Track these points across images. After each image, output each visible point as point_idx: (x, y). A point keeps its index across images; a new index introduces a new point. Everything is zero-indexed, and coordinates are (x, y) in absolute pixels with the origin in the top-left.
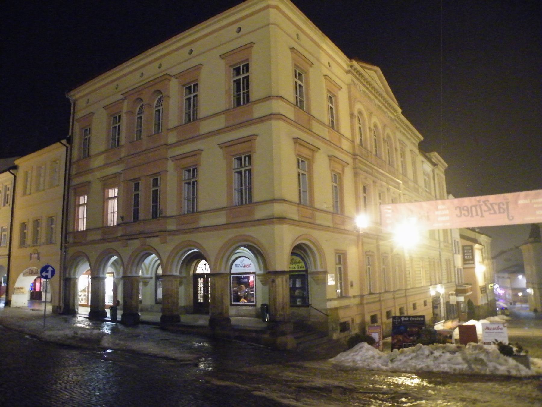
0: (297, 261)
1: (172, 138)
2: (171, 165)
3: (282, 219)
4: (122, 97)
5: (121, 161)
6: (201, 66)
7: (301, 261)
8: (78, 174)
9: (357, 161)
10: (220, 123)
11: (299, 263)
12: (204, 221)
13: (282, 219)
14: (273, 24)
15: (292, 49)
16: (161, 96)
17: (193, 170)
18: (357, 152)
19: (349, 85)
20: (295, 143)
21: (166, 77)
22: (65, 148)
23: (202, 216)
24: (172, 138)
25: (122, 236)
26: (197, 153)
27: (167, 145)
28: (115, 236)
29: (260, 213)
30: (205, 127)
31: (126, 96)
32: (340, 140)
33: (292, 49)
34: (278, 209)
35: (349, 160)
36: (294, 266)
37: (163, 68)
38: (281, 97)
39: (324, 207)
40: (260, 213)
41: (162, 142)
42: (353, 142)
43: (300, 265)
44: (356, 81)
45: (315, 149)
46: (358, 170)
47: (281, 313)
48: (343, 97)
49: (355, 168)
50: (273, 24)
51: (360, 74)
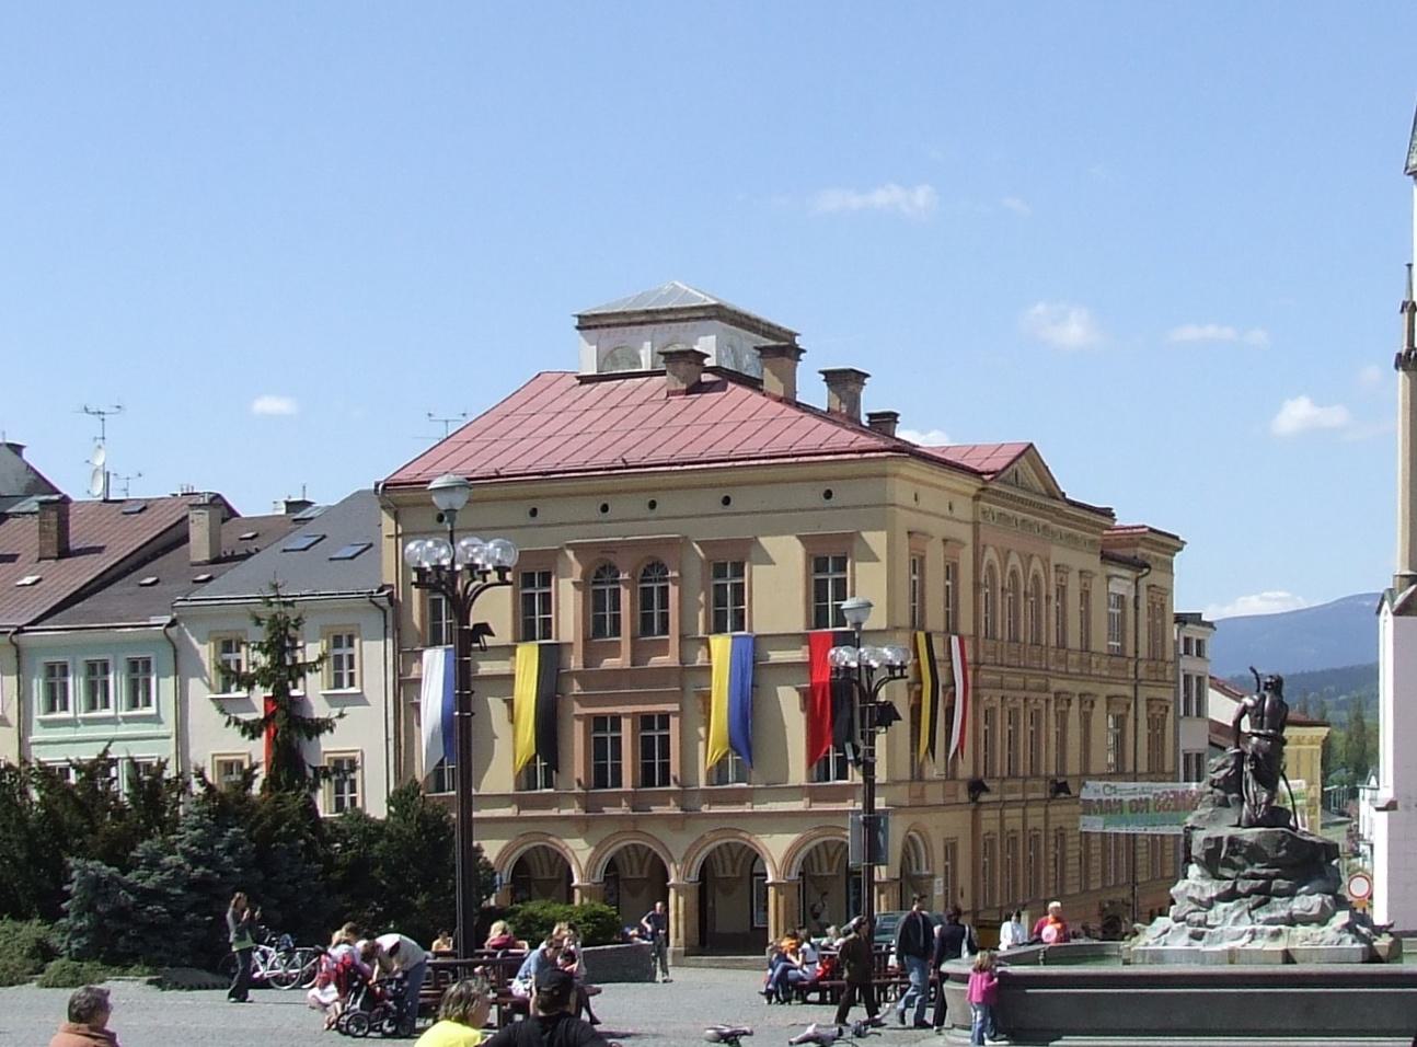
9: (980, 673)
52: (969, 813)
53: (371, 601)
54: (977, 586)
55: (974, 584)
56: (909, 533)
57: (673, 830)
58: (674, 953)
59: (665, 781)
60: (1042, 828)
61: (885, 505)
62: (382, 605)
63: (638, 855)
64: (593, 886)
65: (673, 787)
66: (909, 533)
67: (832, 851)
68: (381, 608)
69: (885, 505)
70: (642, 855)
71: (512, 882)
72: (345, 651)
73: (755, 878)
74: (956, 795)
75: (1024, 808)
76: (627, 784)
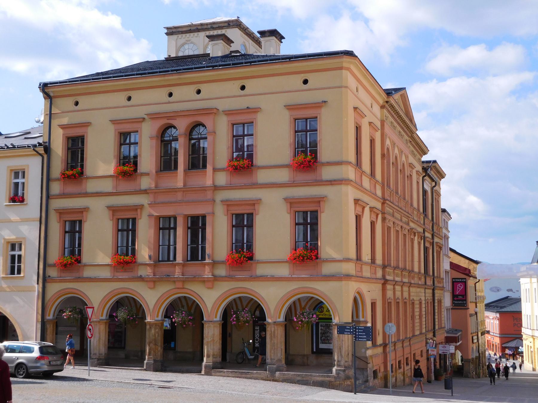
9: (386, 205)
21: (211, 112)
52: (380, 285)
53: (34, 150)
54: (383, 156)
55: (382, 155)
56: (354, 108)
57: (208, 288)
58: (206, 367)
59: (203, 258)
60: (393, 298)
61: (341, 87)
62: (40, 152)
63: (187, 304)
64: (156, 322)
65: (207, 261)
66: (354, 108)
67: (303, 304)
68: (40, 155)
69: (341, 87)
70: (190, 304)
71: (286, 320)
72: (20, 180)
73: (308, 133)
74: (375, 273)
75: (394, 285)
76: (179, 259)
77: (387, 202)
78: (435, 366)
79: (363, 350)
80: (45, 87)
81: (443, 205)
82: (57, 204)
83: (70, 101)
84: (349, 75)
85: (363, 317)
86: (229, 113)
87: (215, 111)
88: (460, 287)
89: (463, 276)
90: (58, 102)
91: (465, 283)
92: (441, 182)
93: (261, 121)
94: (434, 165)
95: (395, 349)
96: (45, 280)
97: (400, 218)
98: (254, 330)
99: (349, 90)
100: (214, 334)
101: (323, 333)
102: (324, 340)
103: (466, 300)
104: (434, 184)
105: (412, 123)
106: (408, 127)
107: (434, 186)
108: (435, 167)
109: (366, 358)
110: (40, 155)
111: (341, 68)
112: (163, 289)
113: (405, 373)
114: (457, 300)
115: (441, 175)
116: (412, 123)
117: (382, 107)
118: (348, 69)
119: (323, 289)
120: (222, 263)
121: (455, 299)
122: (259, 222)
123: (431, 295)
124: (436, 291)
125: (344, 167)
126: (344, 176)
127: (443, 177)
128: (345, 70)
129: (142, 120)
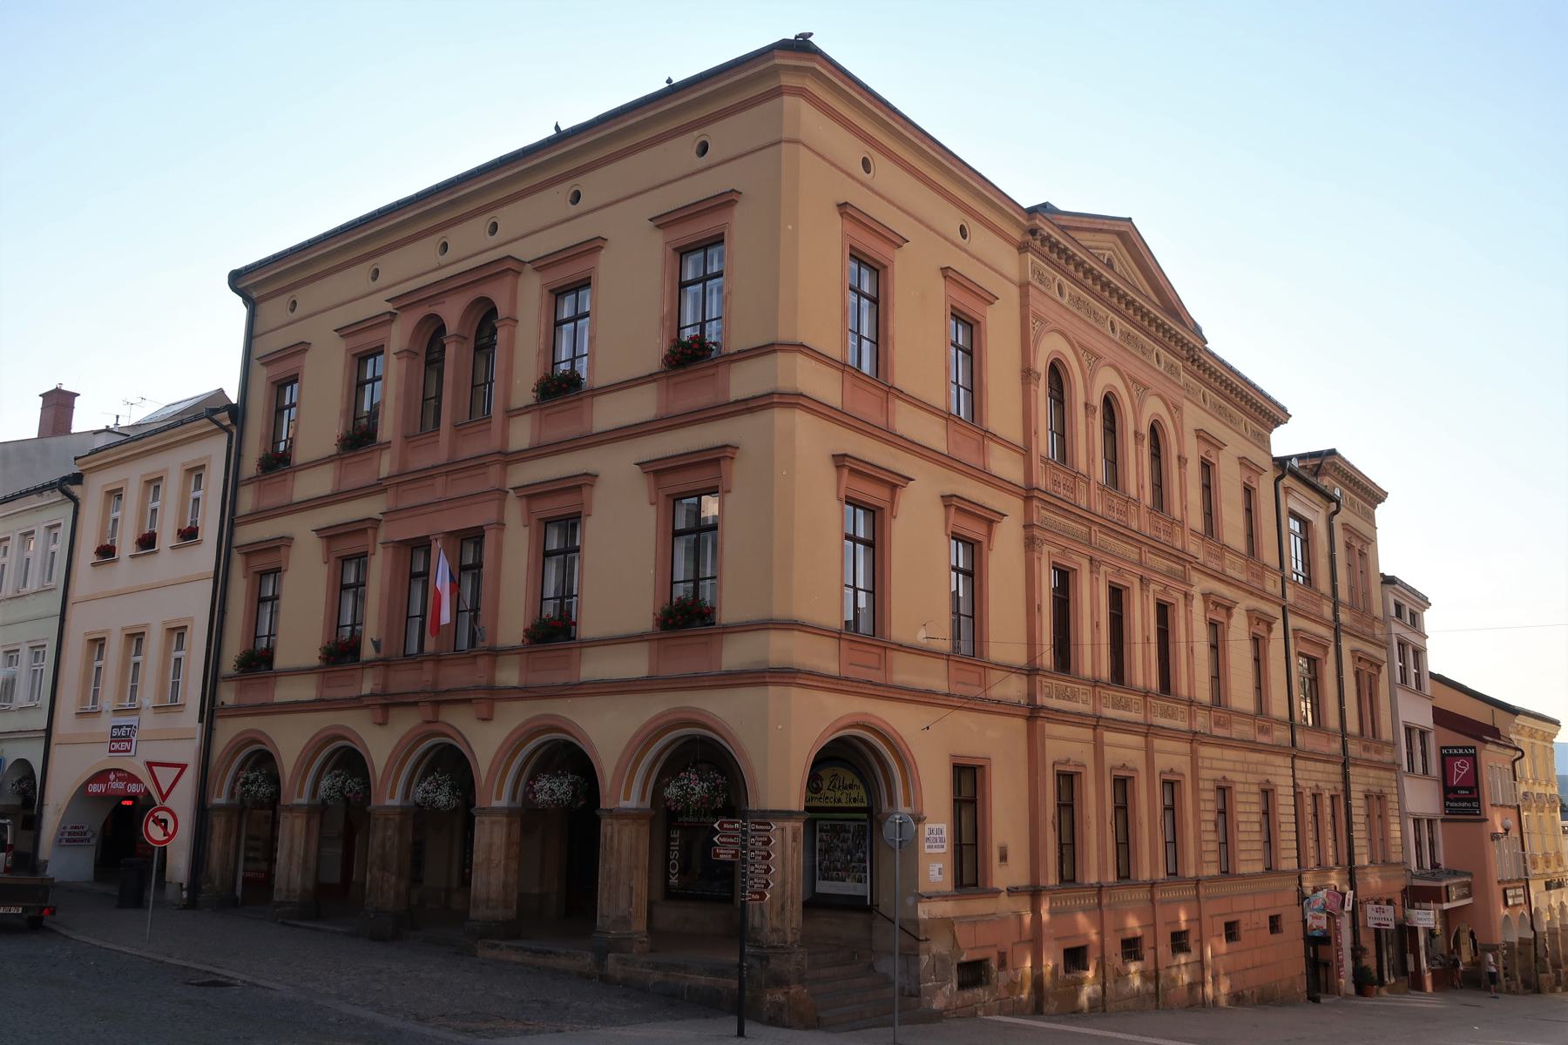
0: (848, 782)
1: (521, 435)
2: (514, 512)
3: (786, 675)
4: (390, 307)
5: (377, 488)
6: (600, 243)
7: (857, 782)
8: (259, 515)
9: (1035, 503)
10: (642, 405)
11: (851, 786)
12: (594, 667)
13: (786, 675)
14: (790, 141)
15: (843, 208)
16: (486, 323)
17: (571, 523)
18: (1041, 480)
19: (1024, 287)
20: (839, 467)
21: (506, 268)
22: (225, 437)
23: (589, 652)
24: (521, 435)
25: (372, 695)
26: (581, 484)
27: (507, 454)
28: (355, 694)
29: (736, 653)
30: (606, 414)
31: (404, 302)
32: (983, 450)
33: (843, 208)
34: (781, 648)
35: (1012, 506)
36: (838, 794)
37: (501, 235)
38: (800, 348)
39: (920, 637)
40: (736, 653)
41: (494, 444)
42: (1026, 451)
43: (854, 793)
44: (1049, 272)
45: (895, 483)
46: (1036, 532)
47: (776, 923)
48: (1000, 327)
49: (1028, 526)
50: (790, 141)
51: (1063, 251)
77: (1036, 493)
78: (1356, 958)
79: (910, 901)
80: (238, 280)
81: (1386, 568)
82: (248, 534)
83: (283, 301)
84: (806, 110)
85: (908, 803)
86: (543, 264)
87: (509, 264)
88: (1460, 769)
89: (1472, 742)
90: (266, 309)
91: (1474, 758)
92: (1377, 512)
93: (605, 268)
94: (1330, 460)
95: (1100, 903)
96: (210, 712)
97: (1136, 557)
98: (669, 840)
99: (802, 149)
100: (490, 845)
101: (827, 851)
102: (828, 869)
103: (1478, 800)
104: (1333, 506)
105: (1184, 324)
106: (1180, 341)
107: (1336, 513)
108: (1334, 464)
109: (916, 922)
110: (226, 429)
111: (778, 92)
112: (405, 723)
113: (1162, 973)
114: (1457, 800)
115: (1372, 495)
116: (1184, 324)
117: (1022, 248)
118: (801, 92)
119: (725, 711)
120: (511, 650)
121: (1451, 796)
122: (592, 535)
123: (1339, 778)
124: (1352, 770)
125: (782, 359)
126: (783, 385)
127: (1381, 500)
128: (790, 94)
129: (387, 317)
